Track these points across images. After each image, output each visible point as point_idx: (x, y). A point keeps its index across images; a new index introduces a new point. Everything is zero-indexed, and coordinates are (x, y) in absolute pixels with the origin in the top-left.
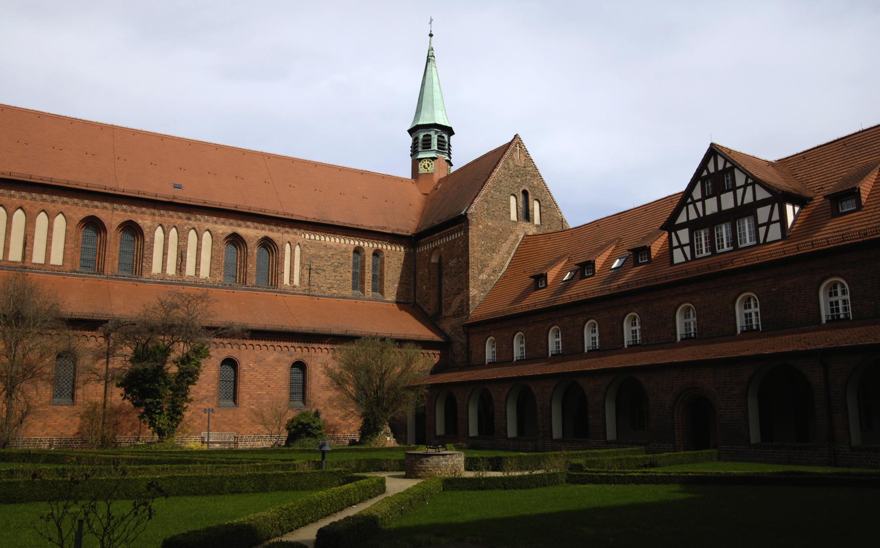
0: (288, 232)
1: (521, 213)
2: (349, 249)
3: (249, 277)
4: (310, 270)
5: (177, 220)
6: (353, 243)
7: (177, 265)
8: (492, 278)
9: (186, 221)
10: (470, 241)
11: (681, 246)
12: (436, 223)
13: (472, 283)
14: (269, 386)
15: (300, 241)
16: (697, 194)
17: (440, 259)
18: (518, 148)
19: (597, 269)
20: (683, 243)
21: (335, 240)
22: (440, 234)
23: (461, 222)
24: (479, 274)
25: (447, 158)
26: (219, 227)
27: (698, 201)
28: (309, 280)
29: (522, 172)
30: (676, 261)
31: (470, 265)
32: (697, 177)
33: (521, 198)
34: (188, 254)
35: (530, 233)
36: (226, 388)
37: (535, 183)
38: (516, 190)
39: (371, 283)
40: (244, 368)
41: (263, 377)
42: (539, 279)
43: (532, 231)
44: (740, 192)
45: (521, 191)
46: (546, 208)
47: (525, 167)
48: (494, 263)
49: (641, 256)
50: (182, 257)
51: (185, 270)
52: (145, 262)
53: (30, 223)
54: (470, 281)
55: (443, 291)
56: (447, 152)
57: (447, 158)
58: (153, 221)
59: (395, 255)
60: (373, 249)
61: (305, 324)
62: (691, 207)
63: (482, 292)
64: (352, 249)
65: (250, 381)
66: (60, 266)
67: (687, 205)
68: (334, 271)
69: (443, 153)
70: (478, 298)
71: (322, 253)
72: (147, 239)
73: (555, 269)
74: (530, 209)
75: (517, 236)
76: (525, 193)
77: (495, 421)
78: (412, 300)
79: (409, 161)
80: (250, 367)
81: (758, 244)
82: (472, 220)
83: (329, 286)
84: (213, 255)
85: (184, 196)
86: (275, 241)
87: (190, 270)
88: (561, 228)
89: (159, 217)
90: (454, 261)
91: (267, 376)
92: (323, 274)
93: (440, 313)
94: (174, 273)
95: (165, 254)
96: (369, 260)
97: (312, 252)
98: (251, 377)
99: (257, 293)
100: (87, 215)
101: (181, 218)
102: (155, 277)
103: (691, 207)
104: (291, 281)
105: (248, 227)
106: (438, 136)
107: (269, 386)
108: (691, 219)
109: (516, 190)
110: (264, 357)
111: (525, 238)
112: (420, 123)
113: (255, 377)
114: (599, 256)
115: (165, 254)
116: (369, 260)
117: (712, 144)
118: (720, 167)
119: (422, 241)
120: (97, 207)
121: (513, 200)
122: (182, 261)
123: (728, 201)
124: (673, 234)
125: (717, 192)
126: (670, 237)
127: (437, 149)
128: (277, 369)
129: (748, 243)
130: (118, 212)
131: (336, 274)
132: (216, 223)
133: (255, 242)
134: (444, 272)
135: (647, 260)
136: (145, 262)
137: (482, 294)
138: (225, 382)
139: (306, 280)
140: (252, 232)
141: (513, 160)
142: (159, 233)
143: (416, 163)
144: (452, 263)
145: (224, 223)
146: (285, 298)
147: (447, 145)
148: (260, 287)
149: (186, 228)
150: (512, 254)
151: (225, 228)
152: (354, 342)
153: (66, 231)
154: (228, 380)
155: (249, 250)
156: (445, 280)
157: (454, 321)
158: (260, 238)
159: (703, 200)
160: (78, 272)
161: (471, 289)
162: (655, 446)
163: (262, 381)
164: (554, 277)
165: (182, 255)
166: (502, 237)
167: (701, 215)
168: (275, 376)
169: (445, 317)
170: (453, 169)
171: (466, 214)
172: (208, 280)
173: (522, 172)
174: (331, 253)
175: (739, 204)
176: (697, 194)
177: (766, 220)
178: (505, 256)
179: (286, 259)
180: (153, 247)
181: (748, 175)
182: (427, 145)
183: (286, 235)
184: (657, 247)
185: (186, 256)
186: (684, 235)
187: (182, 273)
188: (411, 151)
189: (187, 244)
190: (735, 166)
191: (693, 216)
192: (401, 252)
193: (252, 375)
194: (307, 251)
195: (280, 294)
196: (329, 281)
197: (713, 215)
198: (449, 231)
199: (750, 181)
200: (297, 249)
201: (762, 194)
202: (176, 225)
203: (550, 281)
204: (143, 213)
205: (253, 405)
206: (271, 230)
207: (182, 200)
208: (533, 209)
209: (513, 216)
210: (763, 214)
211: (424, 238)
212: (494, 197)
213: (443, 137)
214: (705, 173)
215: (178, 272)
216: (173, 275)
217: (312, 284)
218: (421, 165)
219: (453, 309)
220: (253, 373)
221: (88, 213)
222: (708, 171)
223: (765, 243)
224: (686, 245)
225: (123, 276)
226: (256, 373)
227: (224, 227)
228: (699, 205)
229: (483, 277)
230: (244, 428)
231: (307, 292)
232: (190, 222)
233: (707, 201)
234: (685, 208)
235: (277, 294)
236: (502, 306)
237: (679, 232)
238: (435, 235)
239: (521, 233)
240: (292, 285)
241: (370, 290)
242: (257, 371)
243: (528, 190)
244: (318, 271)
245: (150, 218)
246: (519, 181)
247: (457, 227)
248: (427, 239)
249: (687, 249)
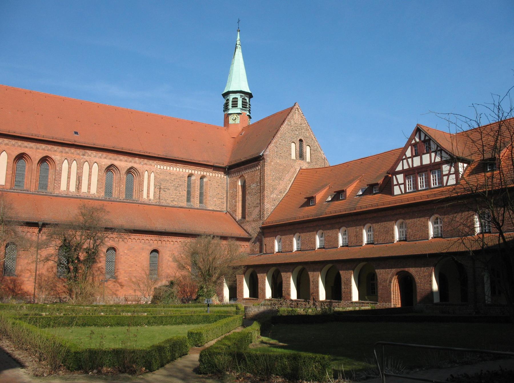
0: (146, 164)
1: (298, 155)
2: (185, 176)
3: (121, 194)
4: (160, 189)
5: (76, 156)
6: (186, 170)
7: (76, 185)
8: (279, 196)
9: (82, 156)
10: (265, 173)
11: (399, 184)
12: (243, 160)
13: (266, 200)
14: (137, 265)
15: (154, 170)
16: (408, 153)
18: (297, 112)
19: (347, 195)
20: (400, 183)
21: (176, 169)
22: (245, 167)
24: (271, 194)
25: (248, 114)
26: (102, 160)
27: (402, 184)
28: (160, 196)
29: (299, 127)
30: (395, 193)
31: (266, 188)
32: (409, 144)
34: (83, 178)
35: (304, 168)
36: (110, 266)
37: (308, 135)
38: (295, 139)
39: (199, 198)
40: (121, 254)
41: (133, 260)
42: (310, 200)
43: (305, 166)
45: (298, 140)
46: (314, 151)
47: (301, 124)
49: (375, 189)
50: (79, 180)
51: (81, 188)
52: (56, 183)
53: (80, 168)
54: (265, 198)
55: (247, 204)
56: (248, 109)
57: (248, 114)
58: (62, 156)
60: (201, 176)
61: (159, 226)
62: (405, 161)
63: (273, 206)
64: (187, 176)
65: (125, 262)
66: (3, 185)
67: (403, 160)
68: (175, 190)
69: (245, 110)
70: (270, 210)
71: (167, 178)
73: (321, 193)
74: (304, 151)
75: (296, 169)
76: (301, 140)
77: (283, 289)
78: (225, 209)
79: (222, 114)
80: (125, 252)
81: (443, 186)
82: (268, 160)
83: (172, 199)
84: (99, 179)
85: (79, 140)
86: (138, 169)
87: (84, 188)
88: (323, 164)
89: (65, 154)
90: (254, 185)
91: (135, 259)
92: (168, 191)
94: (74, 191)
95: (69, 178)
97: (161, 177)
98: (125, 259)
99: (126, 204)
100: (20, 153)
101: (79, 154)
102: (62, 193)
103: (405, 161)
104: (148, 196)
105: (121, 160)
106: (242, 99)
107: (137, 265)
108: (405, 168)
109: (295, 139)
110: (134, 246)
111: (301, 170)
113: (128, 259)
114: (349, 187)
115: (69, 178)
117: (418, 125)
118: (422, 139)
119: (232, 170)
120: (26, 147)
121: (293, 145)
122: (79, 182)
124: (394, 177)
127: (241, 108)
128: (141, 255)
130: (39, 151)
131: (177, 192)
132: (101, 157)
133: (125, 170)
134: (247, 192)
135: (378, 192)
136: (56, 183)
137: (272, 207)
138: (109, 263)
139: (157, 196)
141: (294, 119)
142: (65, 164)
145: (105, 158)
146: (144, 208)
147: (248, 104)
148: (128, 200)
149: (82, 161)
150: (292, 181)
151: (106, 160)
152: (196, 237)
153: (7, 163)
154: (111, 261)
155: (121, 176)
156: (248, 197)
157: (254, 225)
158: (128, 168)
159: (412, 157)
160: (14, 190)
161: (266, 204)
162: (381, 304)
163: (132, 262)
164: (320, 198)
165: (79, 179)
167: (411, 167)
168: (140, 259)
169: (248, 222)
170: (252, 122)
171: (263, 155)
172: (95, 195)
173: (299, 127)
174: (173, 178)
175: (433, 162)
176: (408, 153)
177: (447, 172)
178: (288, 182)
179: (145, 181)
180: (61, 173)
181: (438, 146)
182: (235, 105)
183: (145, 166)
185: (82, 179)
186: (400, 178)
187: (79, 191)
188: (224, 108)
189: (82, 171)
191: (406, 167)
192: (218, 178)
193: (126, 258)
194: (158, 176)
195: (141, 205)
196: (172, 196)
197: (417, 168)
198: (251, 165)
199: (439, 149)
200: (152, 175)
202: (76, 159)
203: (318, 201)
204: (55, 151)
205: (126, 277)
206: (135, 162)
207: (79, 143)
208: (306, 151)
209: (293, 156)
210: (446, 168)
211: (234, 168)
212: (281, 144)
213: (246, 99)
215: (77, 190)
216: (74, 192)
217: (161, 198)
218: (231, 118)
220: (126, 257)
221: (21, 151)
222: (415, 140)
223: (446, 185)
224: (402, 184)
225: (42, 192)
226: (129, 257)
227: (106, 160)
228: (410, 160)
229: (274, 196)
230: (121, 292)
231: (158, 204)
232: (85, 157)
233: (414, 158)
234: (401, 161)
235: (139, 205)
237: (397, 176)
238: (241, 167)
239: (298, 167)
240: (148, 199)
241: (198, 202)
242: (129, 255)
243: (303, 139)
244: (165, 190)
245: (59, 155)
246: (297, 133)
247: (257, 163)
248: (236, 169)
249: (402, 187)
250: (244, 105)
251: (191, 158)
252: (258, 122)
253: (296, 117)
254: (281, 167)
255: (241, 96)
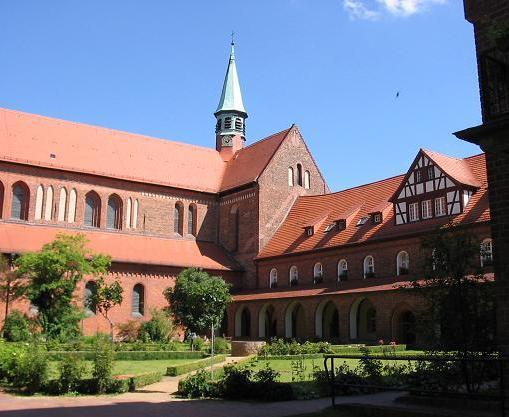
6: (175, 200)
11: (401, 214)
16: (411, 180)
17: (238, 211)
23: (253, 186)
32: (412, 169)
33: (296, 170)
44: (437, 181)
48: (275, 216)
53: (433, 203)
59: (202, 210)
71: (154, 206)
72: (32, 194)
76: (299, 166)
85: (56, 164)
87: (61, 217)
93: (236, 250)
96: (186, 211)
112: (223, 109)
116: (186, 211)
123: (430, 186)
125: (424, 180)
126: (394, 206)
129: (441, 214)
140: (105, 192)
143: (219, 139)
144: (246, 215)
151: (86, 188)
156: (240, 227)
159: (416, 183)
166: (282, 197)
176: (411, 180)
181: (443, 171)
182: (228, 126)
184: (387, 211)
186: (403, 206)
190: (435, 164)
191: (409, 195)
201: (450, 184)
209: (291, 184)
210: (450, 196)
214: (417, 167)
219: (246, 248)
228: (413, 187)
233: (418, 186)
236: (281, 248)
251: (131, 175)
252: (254, 145)
253: (293, 140)
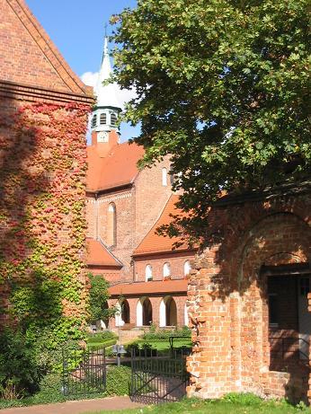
93: (115, 246)
182: (103, 122)
229: (144, 224)
250: (113, 120)
254: (153, 194)
255: (110, 112)
